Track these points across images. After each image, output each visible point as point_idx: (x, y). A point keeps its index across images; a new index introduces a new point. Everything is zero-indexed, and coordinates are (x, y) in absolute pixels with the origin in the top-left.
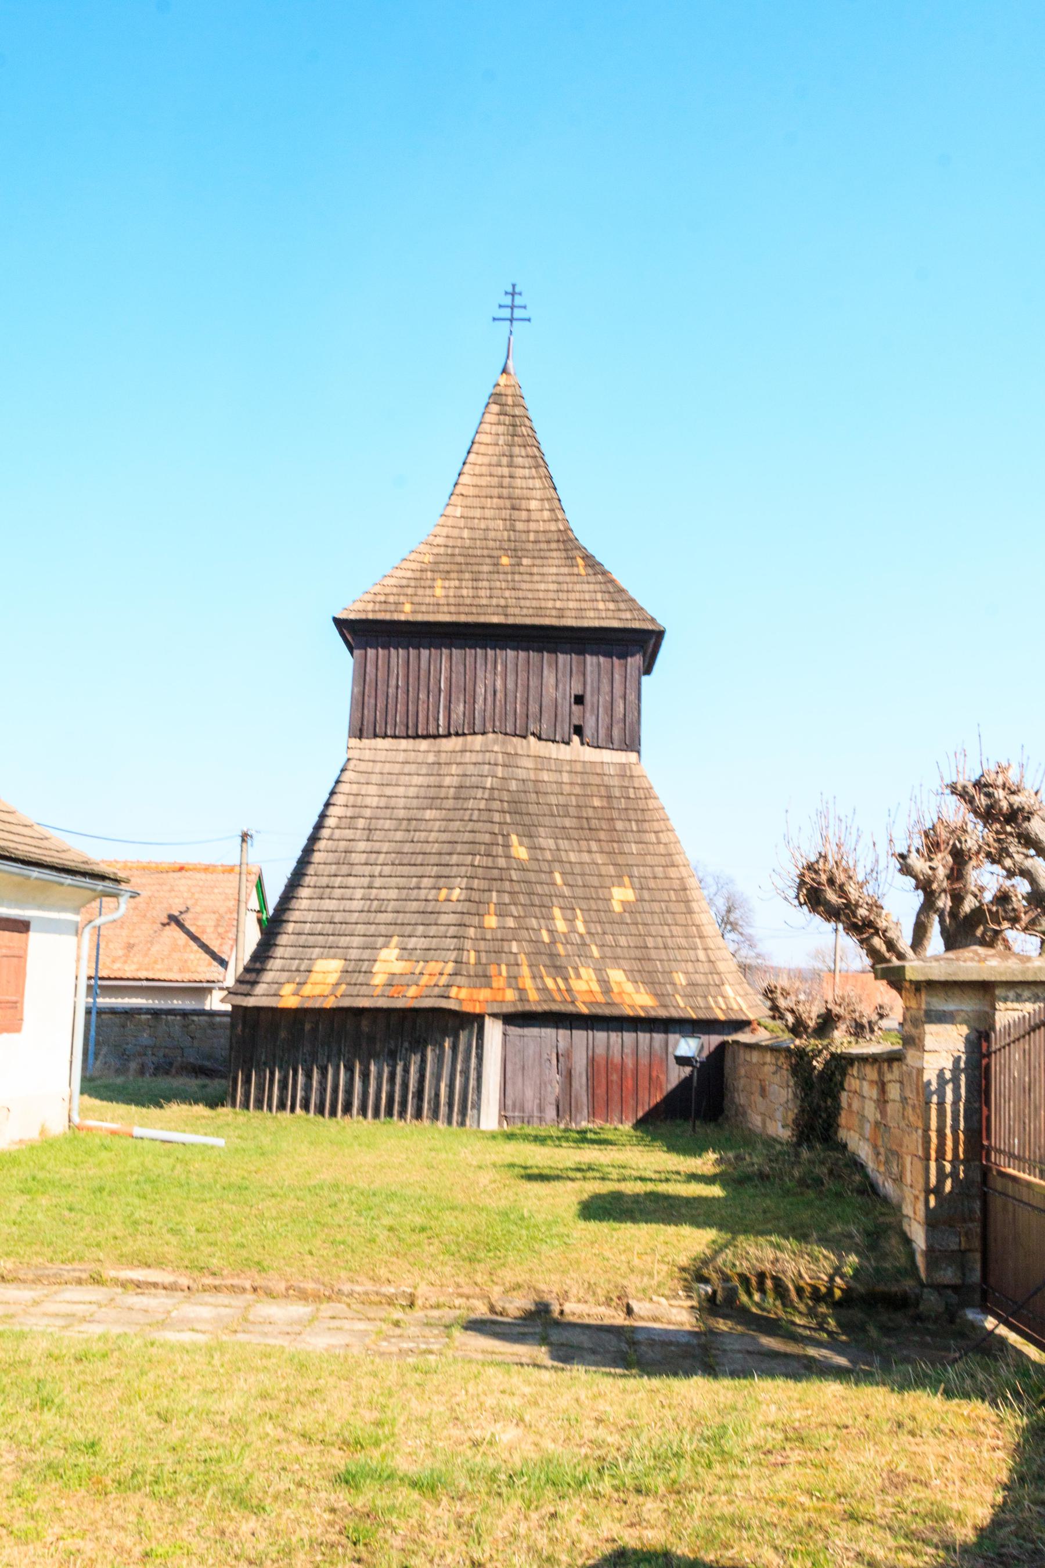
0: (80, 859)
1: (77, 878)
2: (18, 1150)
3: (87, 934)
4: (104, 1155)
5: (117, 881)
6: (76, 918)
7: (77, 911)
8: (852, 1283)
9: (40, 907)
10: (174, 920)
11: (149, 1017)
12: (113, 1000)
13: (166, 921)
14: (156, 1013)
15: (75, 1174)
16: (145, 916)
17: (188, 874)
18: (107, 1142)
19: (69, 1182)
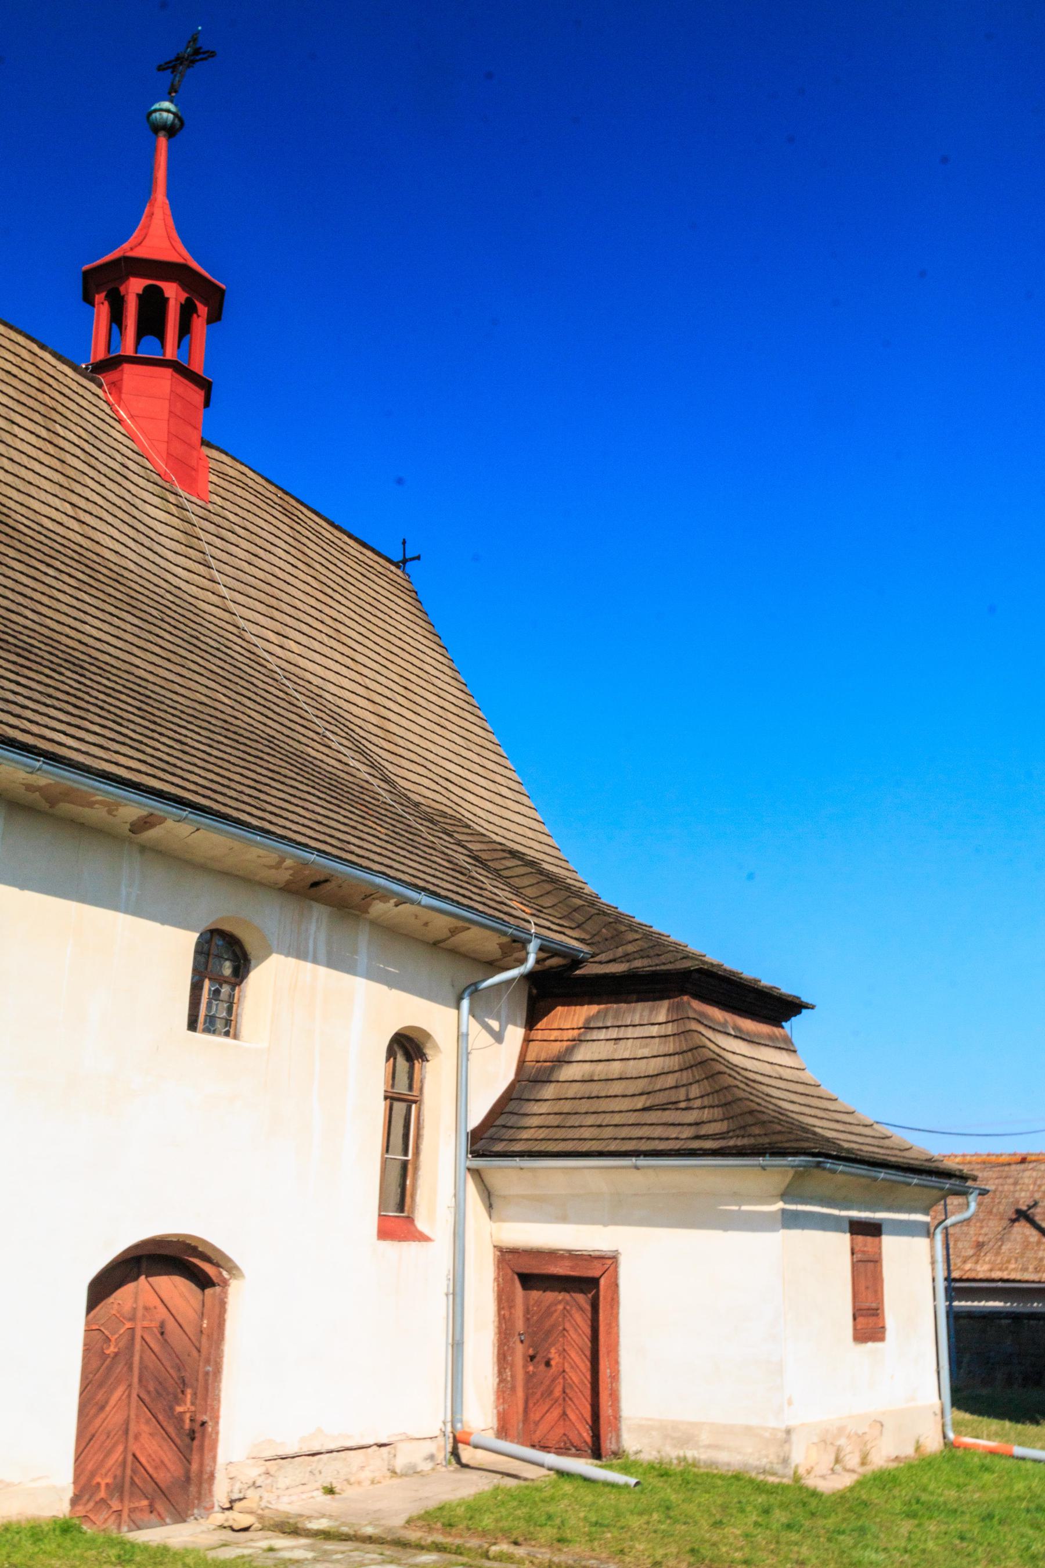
0: (924, 1157)
1: (924, 1177)
2: (896, 1469)
3: (939, 1237)
4: (987, 1477)
5: (964, 1178)
6: (926, 1219)
7: (926, 1211)
8: (503, 1018)
9: (889, 1209)
10: (1023, 1215)
11: (1009, 1321)
12: (969, 1303)
13: (1014, 1217)
14: (1016, 1317)
15: (959, 1498)
16: (990, 1212)
17: (1031, 1166)
18: (987, 1461)
19: (955, 1506)
